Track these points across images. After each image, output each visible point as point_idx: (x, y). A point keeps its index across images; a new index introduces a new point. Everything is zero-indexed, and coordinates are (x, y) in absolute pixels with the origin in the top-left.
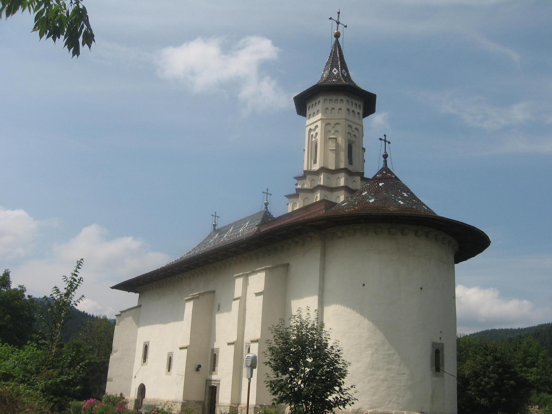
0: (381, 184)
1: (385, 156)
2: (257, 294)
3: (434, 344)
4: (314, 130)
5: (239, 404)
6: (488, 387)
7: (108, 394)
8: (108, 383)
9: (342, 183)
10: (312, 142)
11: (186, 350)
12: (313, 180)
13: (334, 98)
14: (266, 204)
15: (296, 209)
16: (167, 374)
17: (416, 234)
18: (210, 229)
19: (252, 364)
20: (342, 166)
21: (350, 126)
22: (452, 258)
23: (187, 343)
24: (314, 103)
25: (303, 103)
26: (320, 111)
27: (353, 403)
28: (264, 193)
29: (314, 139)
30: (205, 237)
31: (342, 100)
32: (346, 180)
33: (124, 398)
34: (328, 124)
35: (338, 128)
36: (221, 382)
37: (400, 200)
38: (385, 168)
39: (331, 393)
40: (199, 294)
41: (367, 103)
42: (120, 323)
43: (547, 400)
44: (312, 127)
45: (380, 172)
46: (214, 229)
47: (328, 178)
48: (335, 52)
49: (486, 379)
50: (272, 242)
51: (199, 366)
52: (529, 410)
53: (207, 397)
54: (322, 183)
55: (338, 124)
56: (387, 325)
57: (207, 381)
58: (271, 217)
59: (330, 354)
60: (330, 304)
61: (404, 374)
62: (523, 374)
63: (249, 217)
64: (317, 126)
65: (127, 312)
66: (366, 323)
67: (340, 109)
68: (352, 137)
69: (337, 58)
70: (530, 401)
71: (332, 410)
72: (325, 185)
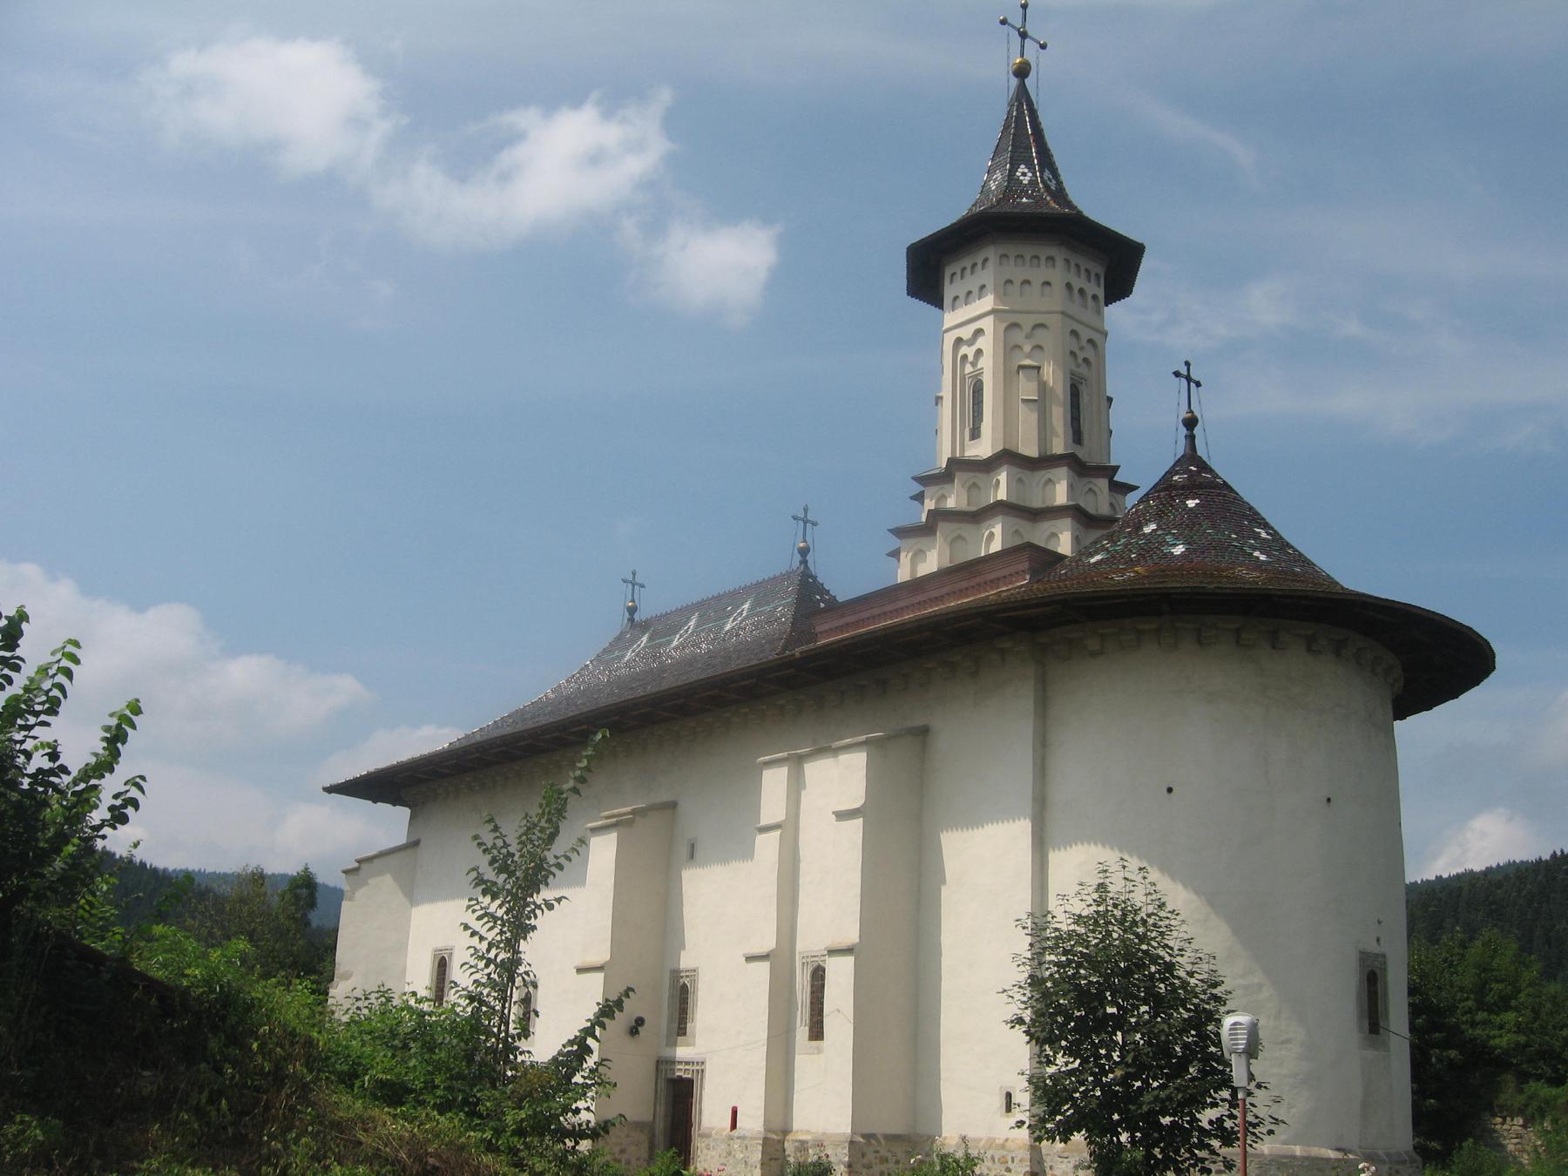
0: (1191, 503)
1: (1191, 423)
2: (842, 816)
3: (1364, 957)
4: (971, 342)
5: (786, 1131)
9: (1060, 494)
13: (1028, 250)
14: (804, 552)
17: (1311, 645)
18: (617, 622)
19: (1249, 1044)
20: (1059, 446)
21: (1074, 333)
23: (602, 955)
26: (990, 287)
28: (795, 518)
29: (968, 369)
31: (1051, 259)
32: (1071, 487)
34: (1014, 325)
35: (1042, 337)
37: (1255, 549)
40: (633, 812)
41: (1115, 262)
42: (359, 894)
43: (1547, 1102)
44: (966, 333)
46: (631, 620)
47: (1020, 480)
48: (1020, 119)
52: (1495, 1131)
53: (661, 1110)
57: (658, 1062)
60: (1068, 842)
61: (1288, 1041)
62: (1478, 1032)
64: (979, 332)
65: (376, 861)
67: (1048, 283)
68: (1078, 366)
69: (1024, 136)
70: (1501, 1107)
72: (1014, 500)
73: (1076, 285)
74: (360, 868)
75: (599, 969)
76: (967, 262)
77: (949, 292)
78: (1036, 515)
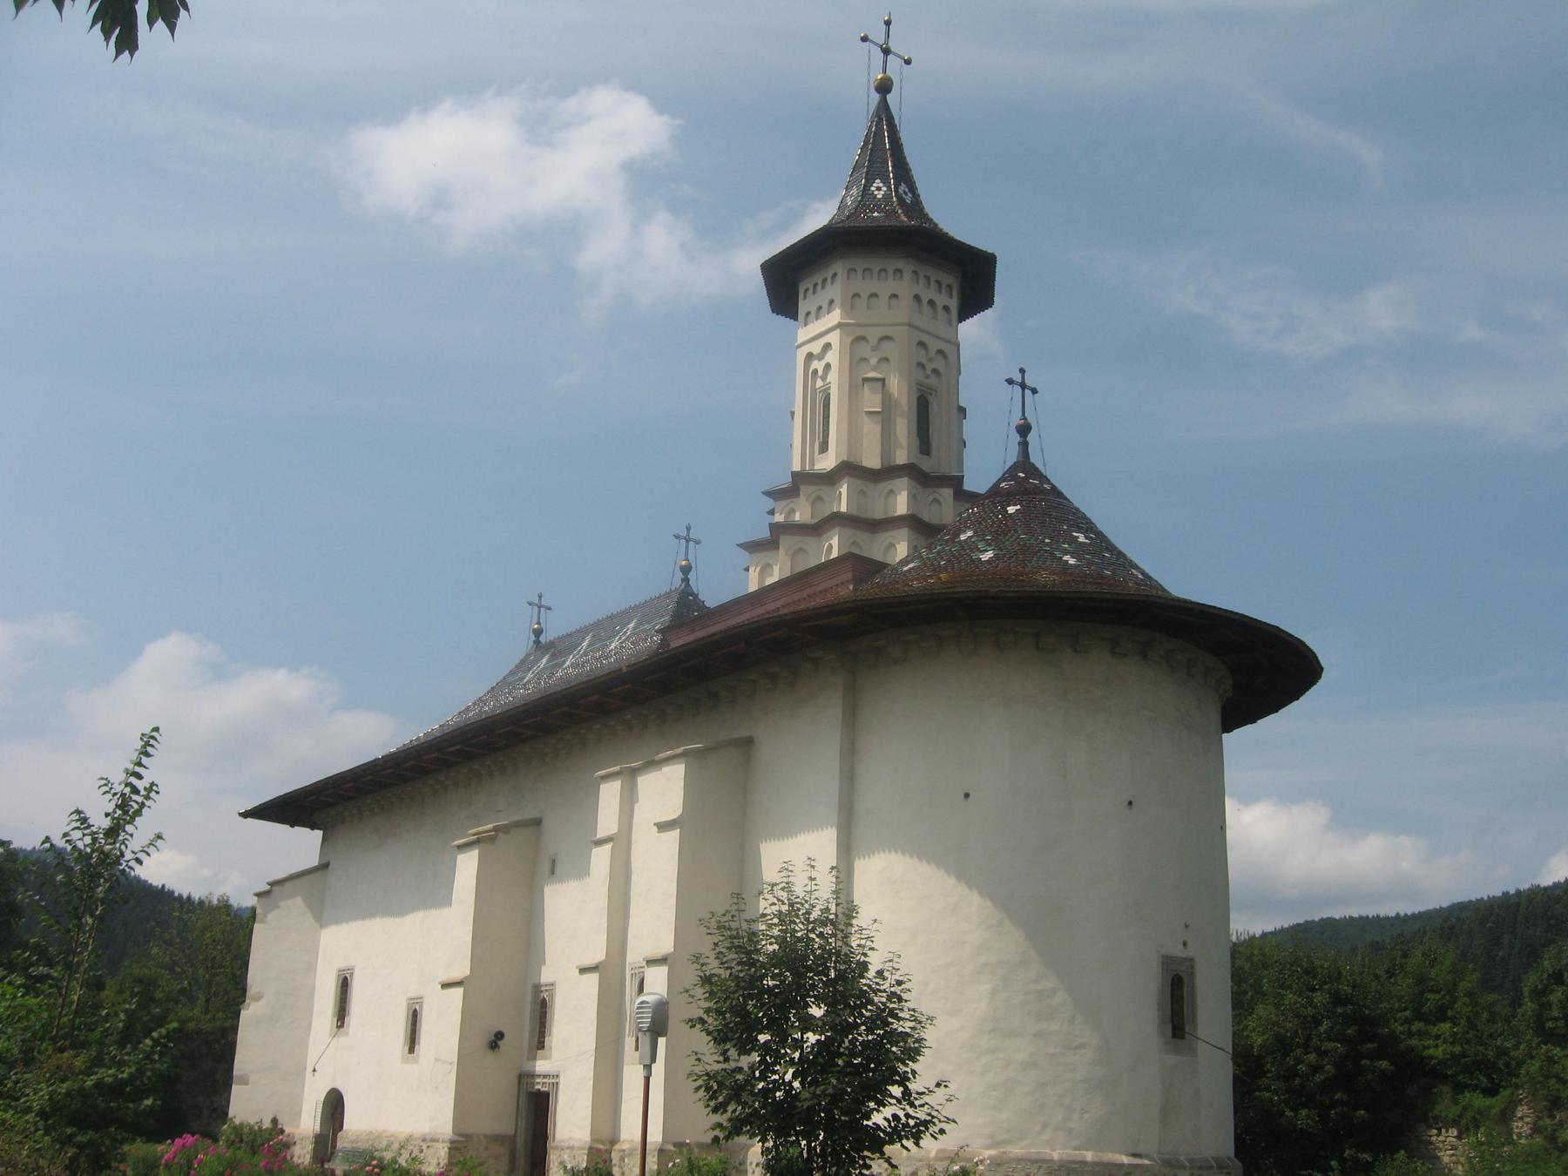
0: (1011, 510)
1: (1024, 430)
2: (663, 827)
3: (1167, 961)
4: (821, 356)
5: (614, 1141)
6: (1319, 1078)
7: (237, 1121)
8: (236, 1089)
9: (901, 505)
10: (814, 390)
11: (459, 991)
12: (819, 498)
13: (876, 264)
14: (686, 570)
15: (770, 581)
16: (405, 1061)
19: (653, 1023)
20: (901, 458)
21: (921, 344)
22: (1215, 717)
23: (462, 970)
24: (818, 278)
25: (788, 279)
26: (838, 301)
27: (942, 1131)
28: (677, 537)
29: (819, 383)
30: (512, 666)
31: (898, 271)
32: (913, 498)
33: (282, 1131)
35: (888, 349)
36: (562, 1082)
37: (1066, 552)
38: (1024, 463)
39: (881, 1104)
40: (496, 829)
42: (269, 917)
43: (1480, 1113)
44: (816, 348)
45: (1011, 473)
46: (537, 642)
47: (862, 492)
48: (878, 135)
49: (1312, 1057)
50: (704, 677)
51: (499, 1036)
53: (522, 1123)
54: (844, 509)
55: (887, 338)
56: (1035, 911)
58: (700, 605)
59: (876, 992)
60: (870, 851)
61: (1082, 1046)
63: (636, 608)
64: (827, 346)
65: (288, 884)
66: (975, 903)
67: (894, 296)
68: (927, 377)
69: (884, 150)
71: (882, 1154)
72: (854, 512)
73: (926, 296)
74: (273, 890)
75: (459, 984)
76: (818, 278)
77: (804, 307)
78: (874, 526)
